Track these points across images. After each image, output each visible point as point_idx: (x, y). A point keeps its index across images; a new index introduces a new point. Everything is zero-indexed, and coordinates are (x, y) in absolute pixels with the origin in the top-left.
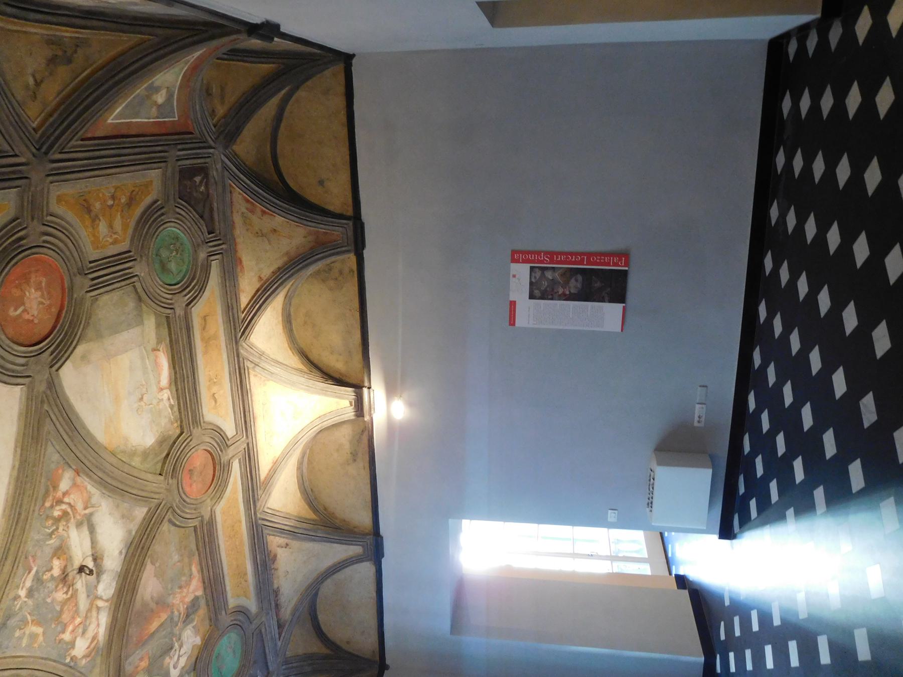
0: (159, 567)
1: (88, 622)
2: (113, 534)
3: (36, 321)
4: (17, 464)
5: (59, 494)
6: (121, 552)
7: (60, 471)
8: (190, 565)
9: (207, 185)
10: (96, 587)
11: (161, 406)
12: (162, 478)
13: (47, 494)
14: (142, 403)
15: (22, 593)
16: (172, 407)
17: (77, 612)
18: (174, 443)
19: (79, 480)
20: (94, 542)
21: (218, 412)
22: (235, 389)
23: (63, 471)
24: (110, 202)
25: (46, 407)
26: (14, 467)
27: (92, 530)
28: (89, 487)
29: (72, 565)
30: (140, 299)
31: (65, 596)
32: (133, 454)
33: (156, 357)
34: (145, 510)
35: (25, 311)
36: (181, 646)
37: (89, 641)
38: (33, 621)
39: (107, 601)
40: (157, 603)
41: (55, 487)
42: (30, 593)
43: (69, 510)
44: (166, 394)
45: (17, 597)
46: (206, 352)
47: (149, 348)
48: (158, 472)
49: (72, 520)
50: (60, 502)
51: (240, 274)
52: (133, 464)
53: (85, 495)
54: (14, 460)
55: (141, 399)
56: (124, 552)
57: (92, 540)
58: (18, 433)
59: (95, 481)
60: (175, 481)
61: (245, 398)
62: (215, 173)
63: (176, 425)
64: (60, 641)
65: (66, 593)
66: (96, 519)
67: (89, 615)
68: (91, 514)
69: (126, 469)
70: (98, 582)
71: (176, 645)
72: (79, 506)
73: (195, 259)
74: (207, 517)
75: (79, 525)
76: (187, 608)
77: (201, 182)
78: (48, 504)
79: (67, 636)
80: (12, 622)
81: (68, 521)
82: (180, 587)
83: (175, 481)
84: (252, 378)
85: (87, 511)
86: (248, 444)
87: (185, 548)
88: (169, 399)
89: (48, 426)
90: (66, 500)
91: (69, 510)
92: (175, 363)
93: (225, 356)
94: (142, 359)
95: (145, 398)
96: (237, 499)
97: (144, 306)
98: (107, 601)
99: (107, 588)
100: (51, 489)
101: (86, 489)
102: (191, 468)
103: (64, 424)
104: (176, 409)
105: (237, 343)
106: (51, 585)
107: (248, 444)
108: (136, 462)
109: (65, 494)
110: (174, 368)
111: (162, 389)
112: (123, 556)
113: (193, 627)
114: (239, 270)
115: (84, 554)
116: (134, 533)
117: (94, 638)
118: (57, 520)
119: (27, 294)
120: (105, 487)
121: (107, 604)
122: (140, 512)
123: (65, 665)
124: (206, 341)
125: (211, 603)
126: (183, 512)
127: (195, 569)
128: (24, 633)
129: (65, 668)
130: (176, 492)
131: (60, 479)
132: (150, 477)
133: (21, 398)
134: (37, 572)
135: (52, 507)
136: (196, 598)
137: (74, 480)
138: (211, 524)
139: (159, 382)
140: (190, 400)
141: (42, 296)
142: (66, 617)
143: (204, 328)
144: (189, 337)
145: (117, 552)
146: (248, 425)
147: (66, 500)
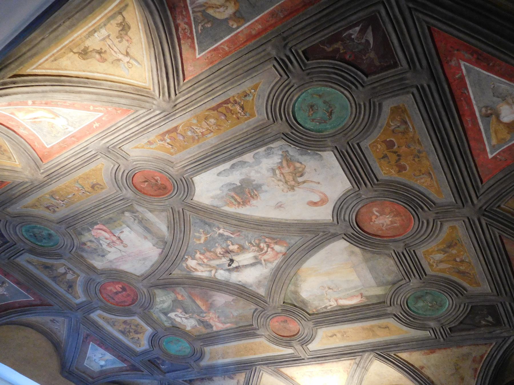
2: (251, 276)
3: (372, 223)
5: (272, 245)
6: (240, 282)
7: (285, 245)
8: (231, 323)
9: (485, 326)
10: (222, 269)
11: (326, 301)
12: (282, 303)
14: (327, 289)
15: (221, 231)
16: (326, 307)
17: (210, 260)
18: (303, 310)
20: (246, 266)
21: (325, 338)
22: (340, 349)
24: (458, 260)
25: (321, 234)
26: (287, 220)
27: (252, 265)
28: (277, 261)
29: (234, 255)
30: (394, 284)
32: (296, 285)
33: (357, 296)
34: (263, 294)
35: (377, 216)
36: (186, 318)
37: (195, 267)
38: (207, 237)
39: (214, 276)
40: (211, 304)
41: (276, 243)
42: (221, 235)
43: (264, 251)
44: (334, 304)
45: (219, 228)
46: (363, 329)
47: (362, 291)
48: (285, 301)
50: (268, 246)
51: (423, 352)
52: (290, 286)
53: (272, 259)
55: (329, 288)
56: (240, 283)
58: (305, 221)
60: (280, 311)
61: (335, 357)
62: (498, 332)
63: (314, 311)
65: (220, 254)
66: (259, 267)
68: (261, 264)
69: (287, 282)
70: (225, 270)
71: (187, 316)
72: (266, 257)
73: (429, 319)
74: (258, 332)
75: (256, 257)
76: (207, 322)
77: (488, 321)
78: (267, 240)
79: (198, 255)
80: (207, 227)
81: (258, 251)
82: (218, 317)
83: (280, 311)
84: (349, 362)
85: (263, 261)
86: (303, 359)
87: (241, 319)
88: (330, 306)
89: (310, 236)
91: (264, 251)
92: (354, 308)
93: (362, 342)
94: (355, 288)
95: (330, 291)
96: (268, 352)
97: (390, 286)
98: (214, 276)
99: (221, 275)
102: (288, 322)
103: (312, 244)
104: (325, 310)
105: (372, 350)
106: (224, 245)
107: (303, 359)
108: (291, 288)
110: (351, 308)
111: (336, 301)
112: (238, 283)
114: (426, 351)
115: (240, 261)
116: (250, 288)
117: (196, 270)
118: (258, 246)
119: (387, 217)
120: (276, 270)
121: (213, 275)
122: (262, 292)
123: (184, 256)
124: (371, 329)
125: (208, 336)
126: (262, 317)
127: (228, 325)
129: (182, 255)
130: (273, 312)
132: (282, 296)
133: (325, 220)
134: (232, 237)
135: (266, 242)
136: (212, 327)
137: (280, 253)
138: (254, 335)
139: (341, 299)
140: (331, 319)
141: (387, 225)
142: (208, 254)
143: (380, 327)
144: (373, 317)
145: (240, 279)
146: (317, 359)
147: (269, 249)
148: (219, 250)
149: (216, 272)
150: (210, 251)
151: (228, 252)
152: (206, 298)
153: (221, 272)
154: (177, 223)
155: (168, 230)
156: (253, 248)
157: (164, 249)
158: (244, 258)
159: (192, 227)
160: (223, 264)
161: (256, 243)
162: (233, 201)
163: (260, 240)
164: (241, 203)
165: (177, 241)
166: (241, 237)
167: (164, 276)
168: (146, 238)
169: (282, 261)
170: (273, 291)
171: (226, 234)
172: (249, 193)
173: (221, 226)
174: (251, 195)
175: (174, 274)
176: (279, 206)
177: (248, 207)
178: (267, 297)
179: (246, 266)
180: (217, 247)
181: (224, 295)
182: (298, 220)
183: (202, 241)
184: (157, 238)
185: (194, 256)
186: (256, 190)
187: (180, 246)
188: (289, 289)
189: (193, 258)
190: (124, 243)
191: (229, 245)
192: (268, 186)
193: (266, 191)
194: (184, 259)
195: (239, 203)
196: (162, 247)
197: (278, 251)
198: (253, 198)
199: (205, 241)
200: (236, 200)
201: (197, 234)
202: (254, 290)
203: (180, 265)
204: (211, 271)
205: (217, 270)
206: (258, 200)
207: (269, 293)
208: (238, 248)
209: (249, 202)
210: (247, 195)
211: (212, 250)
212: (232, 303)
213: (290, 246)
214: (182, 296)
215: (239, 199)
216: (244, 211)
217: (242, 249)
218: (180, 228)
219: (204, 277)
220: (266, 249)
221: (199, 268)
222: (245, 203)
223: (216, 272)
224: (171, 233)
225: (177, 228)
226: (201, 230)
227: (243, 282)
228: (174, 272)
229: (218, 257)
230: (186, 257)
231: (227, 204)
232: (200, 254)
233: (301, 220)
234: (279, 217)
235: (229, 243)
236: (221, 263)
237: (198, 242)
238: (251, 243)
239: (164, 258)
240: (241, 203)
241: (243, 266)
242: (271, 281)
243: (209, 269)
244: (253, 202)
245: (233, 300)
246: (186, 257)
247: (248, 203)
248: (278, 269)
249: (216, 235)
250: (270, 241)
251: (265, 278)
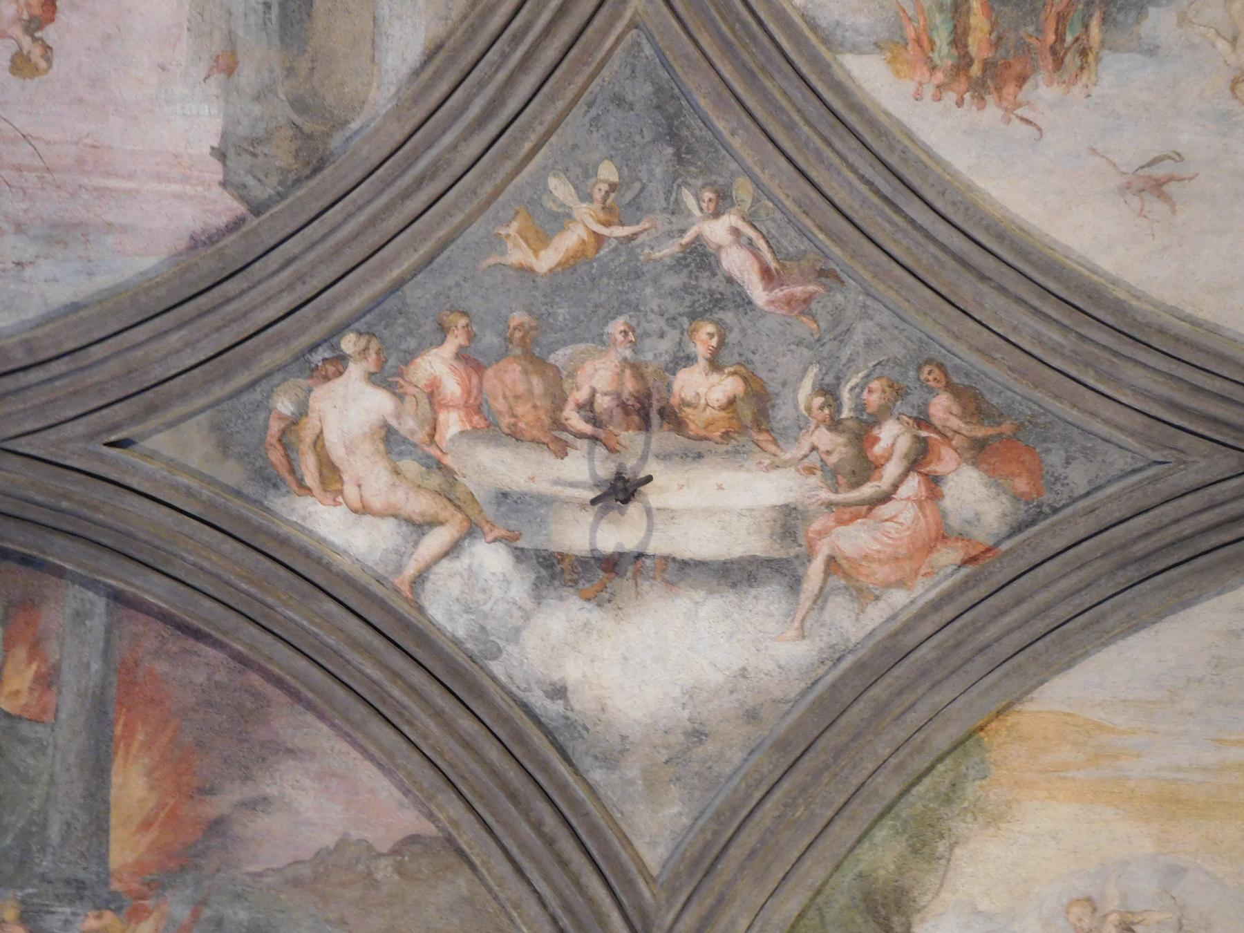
0: (369, 880)
1: (410, 466)
2: (653, 671)
4: (879, 636)
5: (946, 461)
6: (558, 692)
7: (1022, 485)
10: (509, 539)
13: (973, 402)
15: (717, 231)
17: (489, 425)
19: (948, 556)
20: (681, 571)
23: (1017, 497)
27: (733, 575)
28: (899, 598)
29: (665, 457)
31: (582, 395)
32: (926, 842)
34: (654, 857)
37: (337, 452)
38: (599, 239)
39: (420, 579)
40: (217, 826)
41: (978, 451)
42: (700, 257)
43: (867, 490)
45: (723, 201)
49: (826, 495)
50: (919, 458)
52: (880, 834)
53: (882, 572)
54: (1156, 304)
56: (550, 709)
57: (700, 564)
59: (907, 628)
64: (443, 330)
65: (587, 407)
66: (766, 602)
67: (435, 480)
68: (795, 585)
70: (520, 555)
72: (854, 540)
75: (788, 522)
78: (941, 407)
79: (437, 365)
80: (661, 159)
81: (832, 476)
85: (816, 568)
89: (1204, 463)
90: (913, 485)
91: (867, 490)
98: (420, 579)
99: (469, 592)
100: (980, 432)
101: (900, 584)
103: (1188, 527)
108: (883, 854)
109: (934, 482)
112: (537, 700)
113: (503, 254)
115: (671, 515)
116: (597, 775)
117: (330, 472)
118: (862, 433)
120: (860, 666)
121: (411, 569)
122: (655, 829)
128: (587, 197)
131: (995, 476)
134: (744, 303)
135: (922, 420)
137: (961, 536)
142: (509, 378)
145: (571, 672)
148: (599, 376)
149: (453, 550)
150: (536, 361)
151: (649, 409)
152: (221, 750)
153: (490, 558)
154: (517, 40)
155: (417, 72)
156: (824, 438)
157: (257, 210)
158: (711, 504)
159: (578, 116)
160: (545, 501)
161: (860, 407)
162: (942, 37)
163: (899, 392)
164: (975, 70)
165: (408, 178)
166: (804, 327)
167: (70, 443)
168: (227, 65)
169: (936, 605)
170: (749, 838)
171: (736, 262)
172: (1061, 19)
173: (744, 191)
174: (1060, 38)
175: (151, 456)
176: (1154, 184)
177: (992, 111)
178: (674, 891)
179: (681, 571)
180: (602, 341)
181: (368, 774)
182: (1195, 322)
183: (546, 261)
184: (299, 105)
185: (409, 357)
186: (1104, 21)
187: (394, 222)
188: (865, 858)
189: (386, 378)
190: (50, 34)
191: (689, 360)
192: (1183, 20)
193: (1152, 51)
194: (317, 358)
195: (963, 63)
196: (261, 192)
197: (955, 522)
198: (1059, 63)
199: (570, 264)
200: (958, 40)
201: (560, 189)
202: (611, 796)
203: (257, 395)
204: (420, 526)
205: (472, 531)
206: (1077, 90)
207: (703, 862)
208: (731, 402)
209: (1022, 80)
210: (1040, 30)
211: (559, 357)
212: (384, 870)
213: (1048, 498)
214: (47, 680)
215: (977, 45)
216: (955, 136)
217: (753, 420)
218: (510, 82)
219: (344, 564)
220: (892, 470)
221: (369, 475)
222: (987, 76)
223: (453, 550)
224: (416, 100)
225: (482, 85)
226: (608, 172)
227: (582, 703)
228: (161, 442)
229: (559, 425)
230: (349, 343)
231: (896, 45)
232: (461, 355)
233: (1214, 330)
234: (1107, 263)
235: (704, 338)
236: (542, 487)
237: (518, 254)
238: (829, 392)
239: (207, 278)
240: (975, 70)
241: (668, 560)
242: (782, 745)
243: (420, 505)
244: (1043, 92)
245: (413, 839)
246: (349, 343)
247: (1009, 89)
248: (887, 657)
249: (670, 249)
250: (955, 423)
251: (752, 716)
